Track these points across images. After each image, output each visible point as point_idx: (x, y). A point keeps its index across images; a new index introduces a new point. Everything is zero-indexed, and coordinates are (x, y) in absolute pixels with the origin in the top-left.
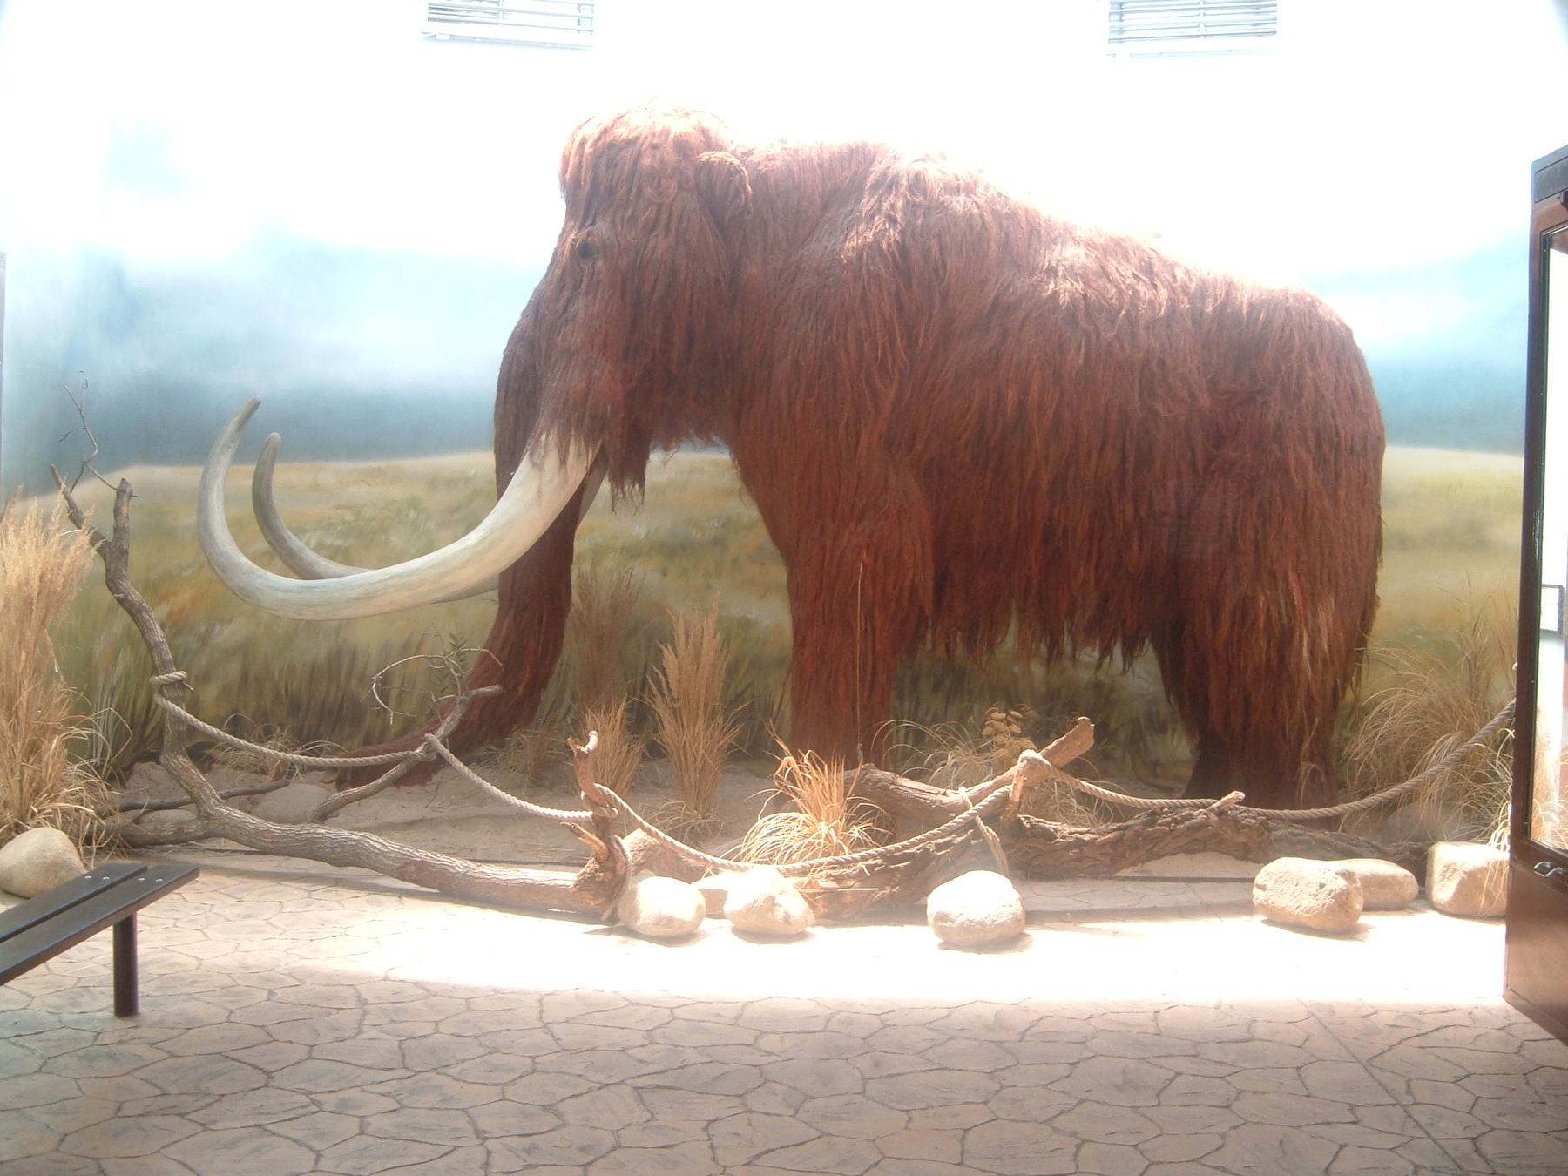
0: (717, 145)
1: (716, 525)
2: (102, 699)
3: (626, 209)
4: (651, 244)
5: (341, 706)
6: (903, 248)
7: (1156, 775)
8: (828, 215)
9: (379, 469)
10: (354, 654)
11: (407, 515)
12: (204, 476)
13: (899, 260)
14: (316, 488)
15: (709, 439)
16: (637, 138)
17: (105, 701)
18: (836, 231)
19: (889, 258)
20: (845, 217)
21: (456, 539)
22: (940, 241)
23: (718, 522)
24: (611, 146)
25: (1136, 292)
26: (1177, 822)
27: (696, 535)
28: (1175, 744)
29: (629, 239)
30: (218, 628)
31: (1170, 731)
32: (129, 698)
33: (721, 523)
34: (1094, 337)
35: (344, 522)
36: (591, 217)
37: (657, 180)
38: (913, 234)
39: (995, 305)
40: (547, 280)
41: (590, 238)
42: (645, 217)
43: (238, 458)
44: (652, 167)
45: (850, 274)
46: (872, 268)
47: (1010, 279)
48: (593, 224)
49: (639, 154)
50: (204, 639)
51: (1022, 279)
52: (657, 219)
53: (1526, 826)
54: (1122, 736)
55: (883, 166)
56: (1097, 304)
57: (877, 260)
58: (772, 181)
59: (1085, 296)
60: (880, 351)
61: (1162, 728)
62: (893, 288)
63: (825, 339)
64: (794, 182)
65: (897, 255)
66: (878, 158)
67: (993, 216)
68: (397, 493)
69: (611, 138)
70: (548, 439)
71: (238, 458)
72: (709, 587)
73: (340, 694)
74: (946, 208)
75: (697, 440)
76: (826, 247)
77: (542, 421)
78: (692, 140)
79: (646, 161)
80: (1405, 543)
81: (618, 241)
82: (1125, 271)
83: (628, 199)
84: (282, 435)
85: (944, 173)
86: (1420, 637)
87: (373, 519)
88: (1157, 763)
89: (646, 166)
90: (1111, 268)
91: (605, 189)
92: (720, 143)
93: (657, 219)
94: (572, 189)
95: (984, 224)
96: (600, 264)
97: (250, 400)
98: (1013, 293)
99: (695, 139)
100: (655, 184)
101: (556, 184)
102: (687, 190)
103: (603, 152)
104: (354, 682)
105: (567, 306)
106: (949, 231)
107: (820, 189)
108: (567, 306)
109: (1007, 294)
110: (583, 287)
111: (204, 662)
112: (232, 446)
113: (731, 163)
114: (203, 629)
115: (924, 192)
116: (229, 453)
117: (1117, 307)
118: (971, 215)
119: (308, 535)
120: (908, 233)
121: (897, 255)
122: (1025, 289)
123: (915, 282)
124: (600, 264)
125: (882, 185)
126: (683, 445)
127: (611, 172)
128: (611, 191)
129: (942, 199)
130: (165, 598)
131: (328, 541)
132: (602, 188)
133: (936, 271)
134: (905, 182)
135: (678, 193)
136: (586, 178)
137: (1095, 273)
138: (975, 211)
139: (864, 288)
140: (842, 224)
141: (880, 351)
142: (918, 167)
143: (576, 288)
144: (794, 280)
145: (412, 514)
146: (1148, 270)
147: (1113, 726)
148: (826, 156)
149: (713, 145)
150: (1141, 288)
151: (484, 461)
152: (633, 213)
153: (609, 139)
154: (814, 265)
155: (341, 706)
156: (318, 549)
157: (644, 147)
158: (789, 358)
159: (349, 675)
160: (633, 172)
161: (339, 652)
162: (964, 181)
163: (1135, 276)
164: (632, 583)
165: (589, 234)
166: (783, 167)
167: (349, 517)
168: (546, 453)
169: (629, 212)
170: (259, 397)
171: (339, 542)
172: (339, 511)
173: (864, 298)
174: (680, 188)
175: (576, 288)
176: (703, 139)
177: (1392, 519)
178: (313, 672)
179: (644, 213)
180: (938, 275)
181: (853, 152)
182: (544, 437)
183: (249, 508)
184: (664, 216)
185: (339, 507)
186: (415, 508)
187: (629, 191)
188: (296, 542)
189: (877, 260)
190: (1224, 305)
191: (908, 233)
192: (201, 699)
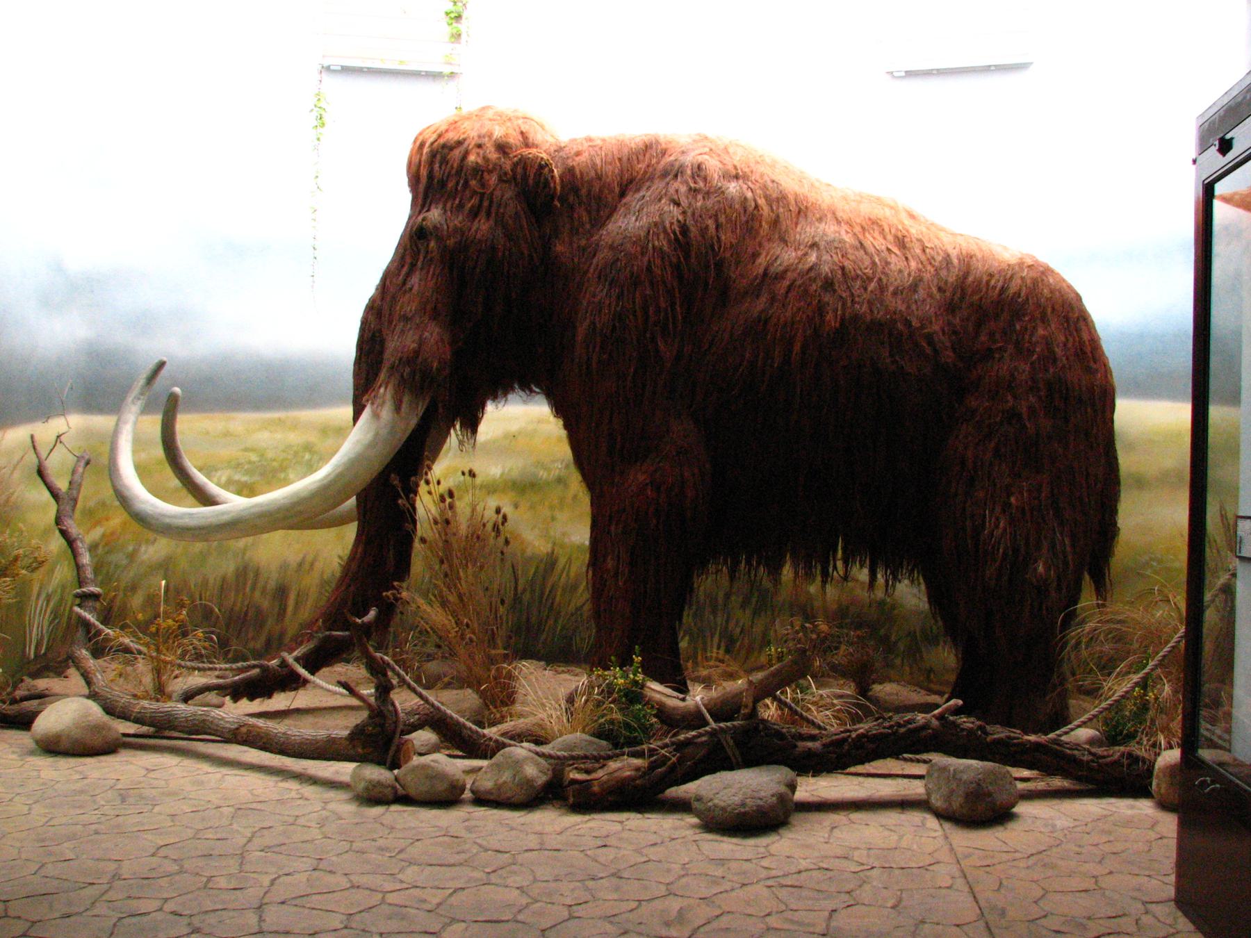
0: (533, 144)
1: (560, 466)
2: (37, 605)
3: (454, 199)
4: (474, 228)
5: (246, 614)
6: (684, 229)
7: (930, 681)
8: (624, 201)
9: (280, 419)
10: (258, 570)
11: (303, 457)
12: (117, 425)
13: (680, 237)
14: (227, 434)
15: (531, 391)
16: (465, 140)
17: (39, 609)
18: (629, 213)
19: (672, 235)
20: (638, 201)
21: (302, 478)
22: (716, 221)
23: (562, 464)
24: (444, 146)
25: (887, 263)
26: (899, 725)
27: (543, 474)
28: (946, 654)
29: (456, 222)
30: (143, 548)
31: (942, 643)
32: (66, 604)
33: (564, 464)
34: (849, 304)
35: (250, 462)
36: (427, 205)
37: (480, 173)
38: (693, 214)
39: (765, 273)
40: (393, 261)
41: (424, 223)
42: (470, 205)
43: (146, 410)
44: (477, 163)
45: (639, 248)
46: (656, 243)
47: (778, 253)
48: (428, 210)
49: (466, 153)
50: (132, 556)
51: (789, 253)
52: (480, 205)
53: (1193, 741)
54: (901, 646)
55: (672, 158)
56: (853, 273)
57: (662, 236)
58: (578, 172)
59: (843, 268)
60: (662, 314)
61: (933, 640)
62: (674, 260)
63: (617, 305)
64: (596, 171)
65: (678, 233)
66: (669, 152)
67: (766, 200)
68: (295, 438)
69: (445, 140)
70: (385, 393)
71: (146, 410)
72: (553, 519)
73: (246, 603)
74: (723, 193)
75: (521, 393)
76: (621, 227)
77: (383, 376)
78: (511, 141)
79: (472, 158)
80: (1141, 483)
81: (447, 225)
82: (875, 242)
83: (456, 189)
84: (182, 391)
85: (724, 164)
86: (1155, 564)
87: (274, 460)
88: (930, 670)
89: (472, 162)
90: (867, 244)
91: (438, 181)
92: (536, 142)
93: (480, 205)
94: (414, 180)
95: (757, 207)
96: (432, 244)
97: (156, 361)
98: (780, 265)
99: (514, 139)
100: (478, 177)
101: (404, 180)
102: (506, 182)
103: (437, 152)
104: (257, 594)
105: (405, 280)
106: (725, 213)
107: (619, 179)
108: (405, 280)
109: (775, 265)
110: (419, 264)
111: (131, 574)
112: (142, 397)
113: (542, 159)
114: (131, 548)
115: (705, 179)
116: (140, 404)
117: (871, 275)
118: (746, 199)
119: (219, 473)
120: (689, 214)
121: (678, 233)
122: (791, 261)
123: (693, 255)
124: (432, 244)
125: (669, 174)
126: (510, 396)
127: (443, 168)
128: (443, 184)
129: (720, 184)
130: (98, 523)
131: (237, 477)
132: (436, 181)
133: (712, 246)
134: (689, 172)
135: (497, 185)
136: (424, 173)
137: (853, 247)
138: (749, 195)
139: (649, 261)
140: (635, 207)
141: (662, 314)
142: (700, 158)
143: (413, 265)
144: (594, 255)
145: (307, 456)
146: (901, 242)
147: (893, 638)
148: (626, 151)
149: (530, 144)
150: (893, 259)
151: (349, 411)
152: (460, 202)
153: (442, 141)
154: (610, 243)
155: (246, 614)
156: (226, 486)
157: (470, 147)
158: (588, 321)
159: (254, 588)
160: (461, 167)
161: (245, 568)
162: (742, 170)
163: (888, 250)
164: (485, 515)
165: (424, 220)
166: (588, 161)
167: (254, 457)
168: (384, 402)
169: (457, 202)
170: (165, 359)
171: (244, 479)
172: (246, 453)
173: (649, 269)
174: (500, 180)
175: (413, 265)
176: (521, 139)
177: (1126, 462)
178: (222, 587)
179: (469, 201)
180: (713, 249)
181: (647, 147)
182: (382, 390)
183: (159, 452)
184: (486, 204)
185: (246, 450)
186: (310, 451)
187: (457, 184)
188: (200, 478)
189: (662, 236)
190: (966, 274)
191: (689, 214)
192: (129, 605)
